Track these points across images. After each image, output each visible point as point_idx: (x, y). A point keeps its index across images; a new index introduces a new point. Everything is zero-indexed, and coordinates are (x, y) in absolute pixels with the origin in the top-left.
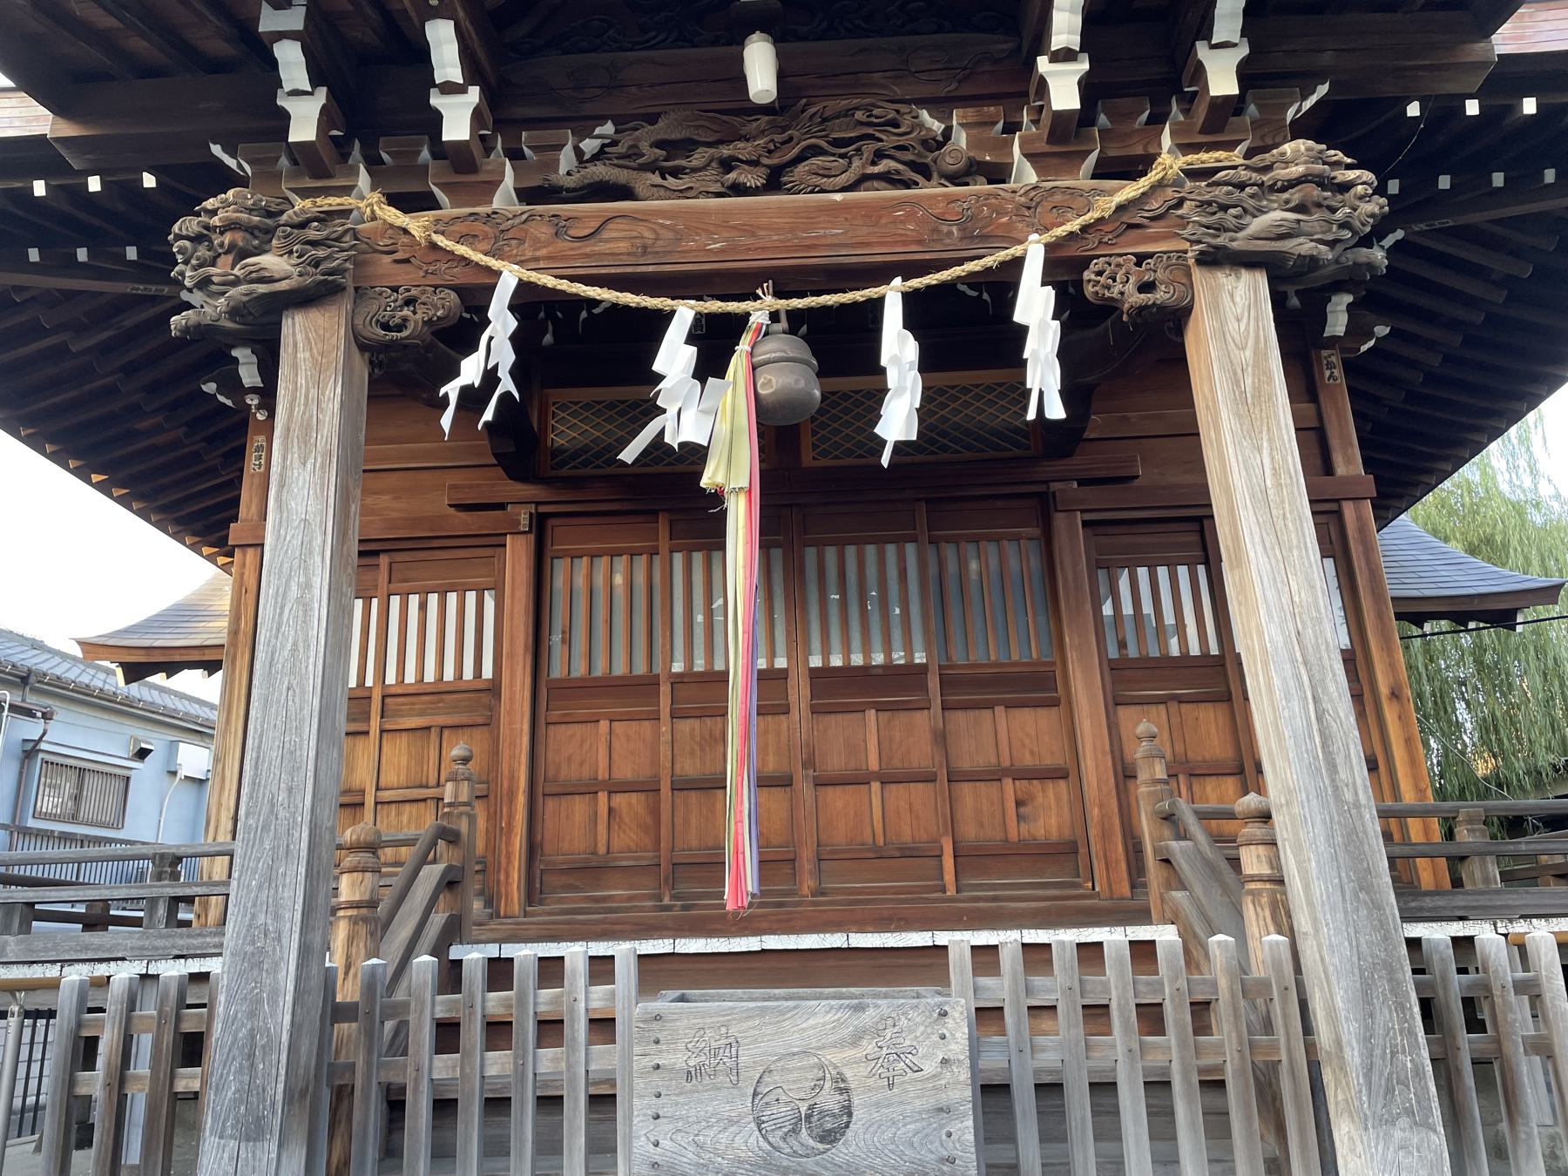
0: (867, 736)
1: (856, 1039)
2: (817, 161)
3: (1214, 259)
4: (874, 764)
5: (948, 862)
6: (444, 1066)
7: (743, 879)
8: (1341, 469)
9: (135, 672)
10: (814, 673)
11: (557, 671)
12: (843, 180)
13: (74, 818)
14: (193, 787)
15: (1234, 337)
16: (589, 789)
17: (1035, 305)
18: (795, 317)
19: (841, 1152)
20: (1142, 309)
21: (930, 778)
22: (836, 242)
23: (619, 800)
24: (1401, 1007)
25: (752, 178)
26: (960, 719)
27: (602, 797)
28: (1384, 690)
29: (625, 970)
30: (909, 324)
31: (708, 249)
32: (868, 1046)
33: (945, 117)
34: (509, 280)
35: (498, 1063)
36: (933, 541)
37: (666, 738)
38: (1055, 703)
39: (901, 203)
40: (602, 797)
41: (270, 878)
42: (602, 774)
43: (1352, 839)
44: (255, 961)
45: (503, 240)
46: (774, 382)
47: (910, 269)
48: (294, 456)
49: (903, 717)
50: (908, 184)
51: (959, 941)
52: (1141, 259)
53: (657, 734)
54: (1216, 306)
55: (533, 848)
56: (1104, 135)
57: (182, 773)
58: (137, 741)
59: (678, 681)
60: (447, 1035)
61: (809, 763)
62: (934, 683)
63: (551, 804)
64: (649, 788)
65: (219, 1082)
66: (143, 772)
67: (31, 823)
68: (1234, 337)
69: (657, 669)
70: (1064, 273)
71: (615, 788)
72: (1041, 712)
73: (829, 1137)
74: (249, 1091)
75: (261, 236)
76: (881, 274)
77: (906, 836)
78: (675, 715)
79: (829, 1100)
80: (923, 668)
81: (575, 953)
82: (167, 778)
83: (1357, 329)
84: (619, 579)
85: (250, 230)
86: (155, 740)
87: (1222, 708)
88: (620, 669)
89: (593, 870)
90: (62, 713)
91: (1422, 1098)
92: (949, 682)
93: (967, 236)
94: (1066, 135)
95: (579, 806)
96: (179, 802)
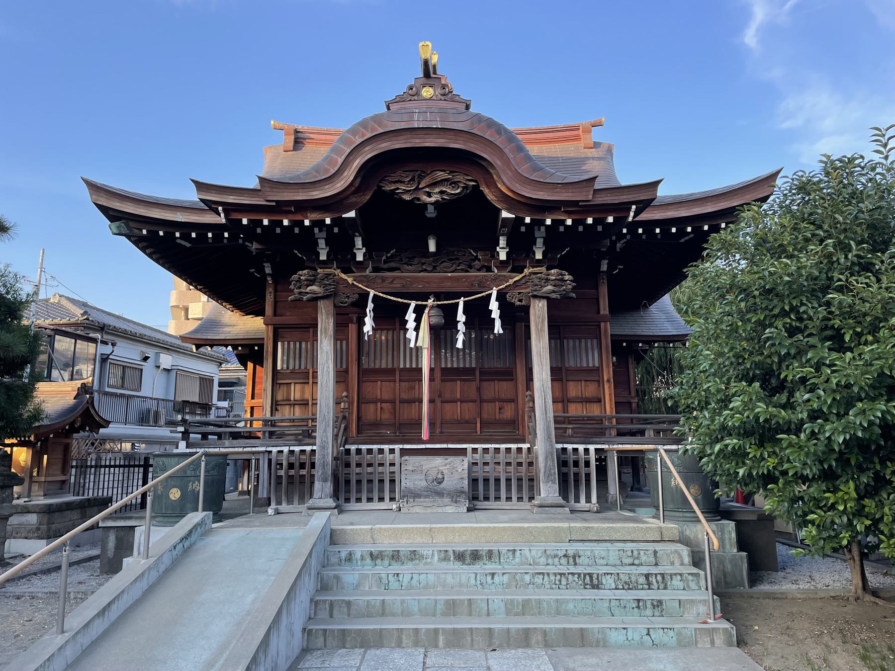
0: (457, 388)
1: (446, 465)
2: (444, 264)
3: (535, 297)
4: (458, 396)
5: (478, 425)
6: (358, 470)
7: (425, 435)
8: (602, 312)
9: (198, 347)
10: (442, 369)
11: (365, 366)
12: (451, 269)
13: (122, 387)
14: (166, 373)
15: (539, 311)
16: (375, 402)
17: (494, 305)
18: (438, 306)
19: (442, 486)
20: (519, 306)
21: (475, 401)
22: (448, 287)
23: (384, 405)
24: (553, 461)
25: (429, 269)
26: (485, 384)
27: (379, 404)
28: (605, 379)
29: (397, 452)
30: (464, 313)
31: (419, 287)
32: (448, 466)
33: (476, 253)
34: (372, 293)
35: (370, 470)
36: (480, 329)
37: (397, 387)
38: (512, 380)
39: (464, 277)
40: (379, 404)
41: (325, 431)
42: (379, 397)
43: (548, 427)
44: (323, 447)
45: (370, 283)
46: (434, 320)
47: (466, 295)
48: (323, 336)
49: (467, 383)
50: (467, 271)
51: (469, 446)
52: (519, 293)
53: (395, 386)
54: (534, 307)
55: (359, 418)
56: (515, 264)
57: (162, 367)
58: (144, 353)
59: (402, 370)
60: (359, 465)
61: (440, 396)
62: (477, 373)
63: (363, 405)
64: (393, 402)
65: (318, 472)
66: (148, 367)
67: (107, 389)
68: (539, 311)
69: (395, 366)
70: (501, 297)
71: (382, 401)
72: (508, 383)
73: (440, 483)
74: (324, 473)
75: (311, 282)
76: (458, 295)
77: (467, 417)
78: (400, 381)
79: (440, 476)
80: (475, 369)
81: (386, 447)
82: (155, 369)
83: (611, 267)
84: (383, 338)
85: (310, 280)
86: (150, 352)
87: (560, 383)
88: (384, 366)
89: (376, 425)
90: (120, 343)
91: (555, 478)
92: (482, 373)
93: (479, 285)
94: (502, 265)
95: (372, 406)
96: (160, 378)
